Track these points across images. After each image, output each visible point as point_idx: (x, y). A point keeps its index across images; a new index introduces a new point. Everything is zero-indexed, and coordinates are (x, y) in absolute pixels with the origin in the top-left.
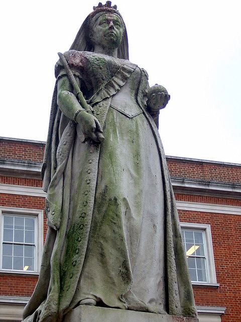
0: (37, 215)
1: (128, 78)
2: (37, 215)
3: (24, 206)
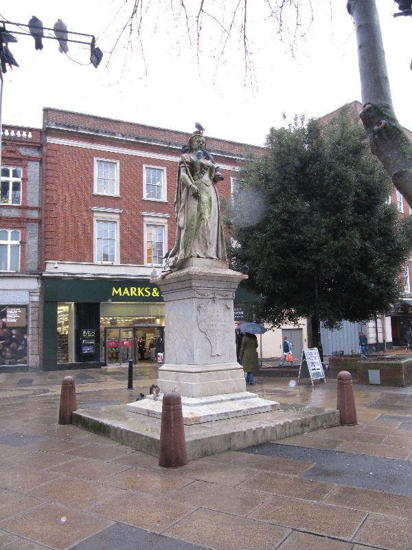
0: (116, 163)
2: (116, 163)
3: (155, 164)
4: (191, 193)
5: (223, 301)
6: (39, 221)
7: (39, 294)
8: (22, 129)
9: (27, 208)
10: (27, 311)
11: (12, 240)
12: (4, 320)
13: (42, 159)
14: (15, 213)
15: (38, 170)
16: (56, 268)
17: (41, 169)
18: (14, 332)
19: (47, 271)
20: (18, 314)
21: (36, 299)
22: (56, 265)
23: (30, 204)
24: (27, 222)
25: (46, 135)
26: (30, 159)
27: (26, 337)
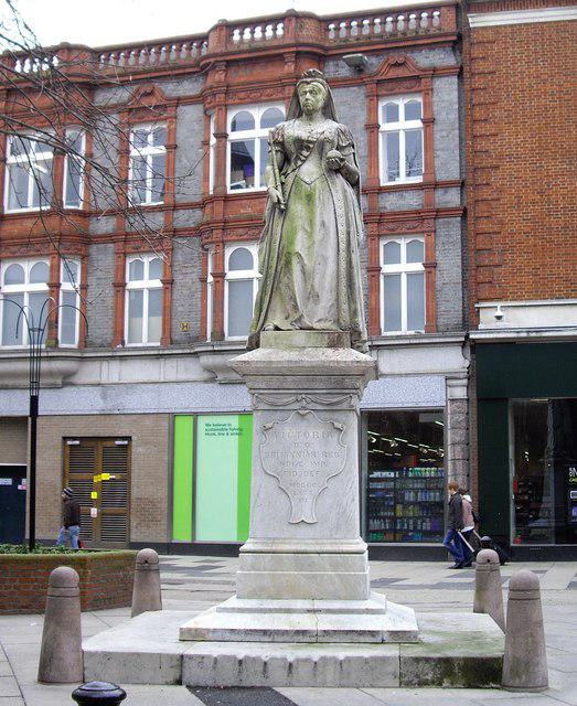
5: (328, 415)
7: (465, 381)
8: (263, 22)
9: (436, 185)
13: (461, 69)
14: (413, 201)
16: (499, 318)
19: (481, 326)
21: (461, 393)
22: (499, 313)
23: (441, 176)
26: (180, 101)
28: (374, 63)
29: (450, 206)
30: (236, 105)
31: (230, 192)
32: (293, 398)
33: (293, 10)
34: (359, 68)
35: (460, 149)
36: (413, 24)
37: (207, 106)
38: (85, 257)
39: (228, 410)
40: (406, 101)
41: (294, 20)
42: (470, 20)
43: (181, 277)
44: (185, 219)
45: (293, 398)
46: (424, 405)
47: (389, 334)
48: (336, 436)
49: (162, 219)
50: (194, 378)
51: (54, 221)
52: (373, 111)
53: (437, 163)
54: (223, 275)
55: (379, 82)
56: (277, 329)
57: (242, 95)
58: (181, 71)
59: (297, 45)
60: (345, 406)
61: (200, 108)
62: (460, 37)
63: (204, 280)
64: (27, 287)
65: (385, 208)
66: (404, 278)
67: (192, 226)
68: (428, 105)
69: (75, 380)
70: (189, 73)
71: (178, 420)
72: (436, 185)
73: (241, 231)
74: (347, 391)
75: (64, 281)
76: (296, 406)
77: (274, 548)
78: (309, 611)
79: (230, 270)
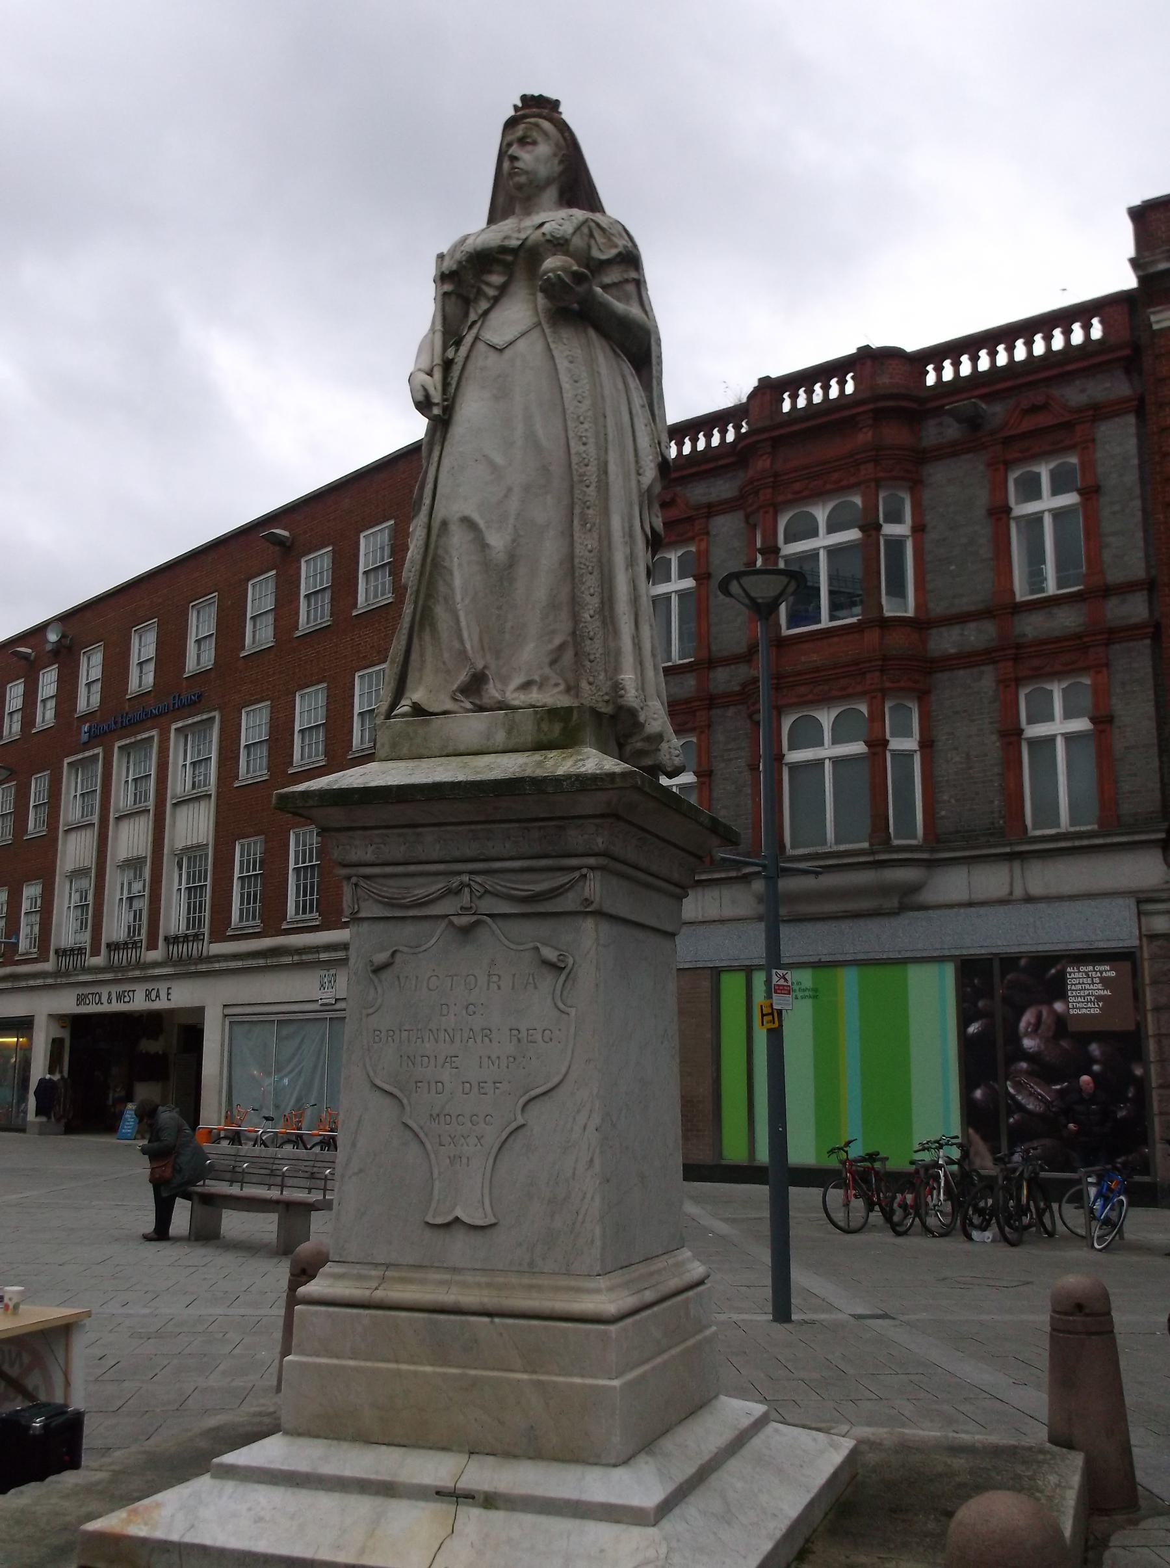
1: (513, 263)
4: (707, 860)
5: (528, 929)
6: (1154, 631)
8: (1063, 318)
9: (1107, 591)
10: (1135, 973)
11: (835, 741)
12: (1058, 1006)
13: (1141, 400)
14: (1068, 620)
15: (1131, 444)
17: (1142, 438)
18: (1095, 1049)
20: (1105, 982)
23: (1115, 576)
24: (1108, 643)
25: (1149, 306)
26: (711, 510)
27: (1138, 1072)
28: (996, 412)
29: (1133, 621)
30: (789, 504)
31: (786, 632)
32: (439, 885)
33: (768, 377)
34: (974, 422)
35: (1145, 531)
36: (730, 437)
37: (749, 510)
38: (923, 696)
39: (795, 960)
40: (1052, 465)
41: (869, 363)
42: (1153, 318)
43: (722, 765)
44: (723, 679)
45: (439, 885)
46: (1102, 945)
47: (1038, 833)
48: (547, 981)
49: (693, 682)
50: (741, 912)
51: (872, 637)
52: (1000, 487)
53: (1107, 555)
54: (780, 757)
55: (1008, 441)
56: (418, 710)
57: (797, 486)
58: (711, 465)
59: (876, 398)
60: (569, 902)
61: (740, 515)
62: (1137, 349)
63: (754, 768)
64: (829, 751)
65: (1025, 635)
66: (1060, 744)
67: (737, 688)
68: (1088, 465)
69: (927, 896)
70: (722, 467)
71: (725, 977)
72: (1107, 591)
73: (803, 690)
74: (574, 862)
75: (893, 735)
76: (446, 907)
77: (380, 1294)
78: (441, 1494)
79: (790, 749)
